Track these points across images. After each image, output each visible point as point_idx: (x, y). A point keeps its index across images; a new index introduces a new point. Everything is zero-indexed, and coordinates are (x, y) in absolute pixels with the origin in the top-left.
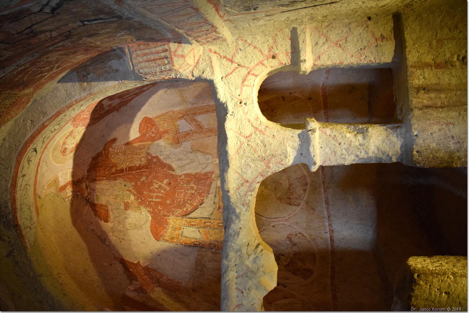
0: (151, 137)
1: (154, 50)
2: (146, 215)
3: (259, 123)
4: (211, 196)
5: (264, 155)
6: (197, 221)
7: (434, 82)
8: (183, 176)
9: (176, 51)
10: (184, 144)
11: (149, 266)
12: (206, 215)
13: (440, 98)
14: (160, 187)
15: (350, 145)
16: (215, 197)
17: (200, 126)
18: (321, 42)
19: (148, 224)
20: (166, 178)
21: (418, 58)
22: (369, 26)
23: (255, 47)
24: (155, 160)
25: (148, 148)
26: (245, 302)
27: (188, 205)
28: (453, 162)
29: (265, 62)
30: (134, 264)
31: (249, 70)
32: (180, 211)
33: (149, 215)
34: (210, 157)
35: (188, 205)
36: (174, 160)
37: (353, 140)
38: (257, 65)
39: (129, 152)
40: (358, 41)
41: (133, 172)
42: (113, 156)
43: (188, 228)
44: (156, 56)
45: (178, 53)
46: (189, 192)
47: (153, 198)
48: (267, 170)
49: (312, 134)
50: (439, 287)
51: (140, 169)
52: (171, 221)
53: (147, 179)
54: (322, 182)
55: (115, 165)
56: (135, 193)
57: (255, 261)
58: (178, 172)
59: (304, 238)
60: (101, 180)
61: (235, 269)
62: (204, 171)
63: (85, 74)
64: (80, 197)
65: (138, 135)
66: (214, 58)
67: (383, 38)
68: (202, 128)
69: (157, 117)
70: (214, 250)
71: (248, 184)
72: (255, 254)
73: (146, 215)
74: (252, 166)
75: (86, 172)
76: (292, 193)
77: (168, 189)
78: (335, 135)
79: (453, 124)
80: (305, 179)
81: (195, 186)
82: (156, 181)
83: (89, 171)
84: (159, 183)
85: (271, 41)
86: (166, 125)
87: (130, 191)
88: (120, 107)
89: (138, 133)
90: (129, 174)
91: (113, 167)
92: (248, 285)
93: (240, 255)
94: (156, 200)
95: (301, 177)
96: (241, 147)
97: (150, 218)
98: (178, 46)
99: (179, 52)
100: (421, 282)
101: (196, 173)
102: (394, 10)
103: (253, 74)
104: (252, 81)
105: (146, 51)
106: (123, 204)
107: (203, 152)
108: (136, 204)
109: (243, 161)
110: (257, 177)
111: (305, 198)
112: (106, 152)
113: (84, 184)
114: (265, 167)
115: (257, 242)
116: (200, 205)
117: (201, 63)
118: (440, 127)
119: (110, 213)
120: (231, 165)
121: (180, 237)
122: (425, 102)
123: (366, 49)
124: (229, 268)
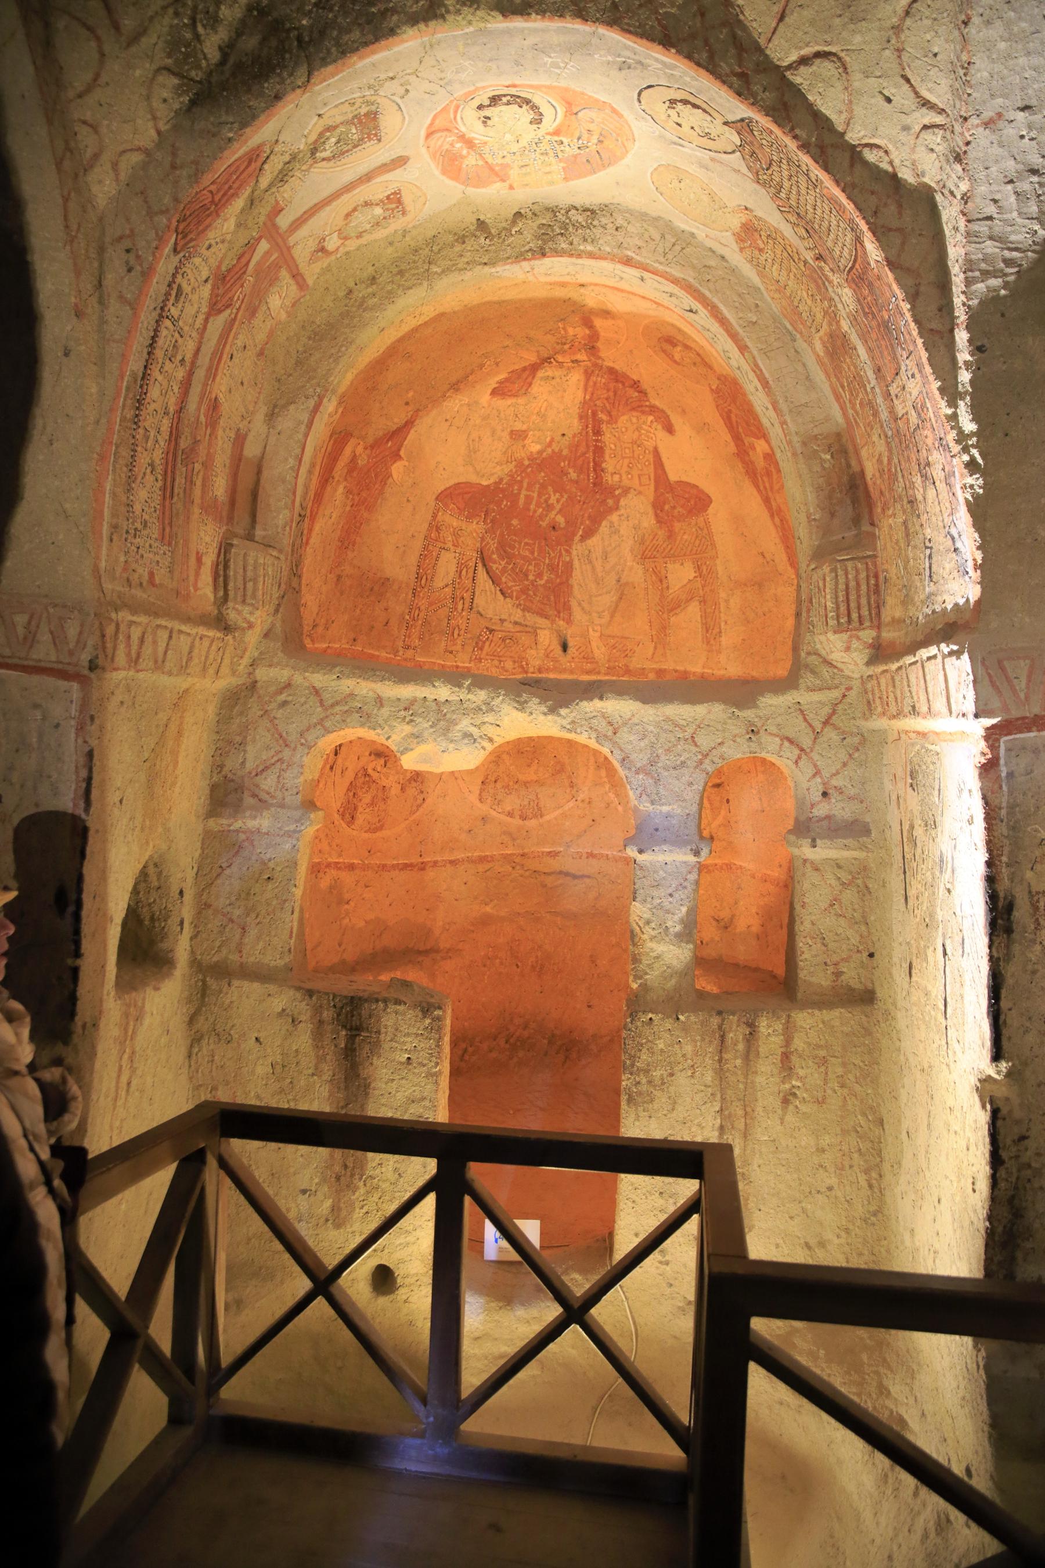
0: (664, 504)
1: (864, 601)
2: (493, 474)
3: (716, 760)
4: (518, 615)
5: (659, 765)
6: (468, 583)
7: (760, 1049)
8: (568, 559)
9: (858, 638)
10: (639, 570)
11: (390, 480)
12: (480, 601)
13: (736, 1058)
14: (550, 507)
15: (668, 912)
16: (516, 623)
17: (676, 606)
18: (842, 874)
19: (473, 479)
20: (567, 522)
21: (802, 1027)
22: (859, 955)
23: (845, 765)
24: (610, 502)
25: (640, 493)
26: (385, 711)
27: (503, 563)
28: (631, 1074)
29: (818, 780)
30: (399, 450)
31: (808, 750)
32: (493, 547)
33: (492, 481)
34: (604, 621)
35: (503, 563)
36: (606, 543)
37: (676, 918)
38: (815, 766)
39: (636, 453)
40: (837, 934)
41: (590, 455)
42: (634, 420)
43: (455, 561)
44: (853, 605)
45: (854, 641)
46: (530, 567)
47: (528, 490)
48: (633, 769)
49: (691, 850)
50: (419, 1048)
51: (595, 470)
52: (474, 526)
53: (571, 480)
54: (526, 851)
55: (612, 420)
56: (545, 454)
57: (467, 735)
58: (578, 549)
59: (415, 808)
60: (586, 389)
61: (454, 698)
62: (574, 603)
63: (833, 450)
64: (558, 347)
65: (673, 477)
66: (836, 694)
67: (838, 974)
68: (672, 610)
69: (707, 523)
70: (407, 617)
71: (610, 733)
72: (481, 737)
73: (493, 474)
74: (642, 744)
75: (611, 364)
76: (507, 787)
77: (544, 524)
78: (685, 887)
79: (692, 1077)
80: (535, 816)
81: (542, 582)
82: (564, 499)
83: (611, 371)
84: (558, 507)
85: (853, 792)
86: (685, 537)
87: (550, 445)
88: (743, 462)
89: (676, 479)
90: (588, 446)
91: (609, 414)
92: (421, 720)
93: (481, 709)
94: (522, 496)
95: (539, 809)
96: (676, 726)
97: (485, 483)
98: (865, 643)
99: (855, 644)
100: (428, 1021)
101: (570, 587)
102: (879, 994)
103: (799, 758)
104: (789, 755)
105: (864, 587)
106: (525, 427)
107: (617, 606)
108: (521, 454)
109: (651, 728)
110: (621, 750)
111: (494, 813)
112: (647, 409)
113: (585, 358)
114: (639, 765)
115: (496, 738)
116: (501, 590)
117: (830, 670)
118: (689, 1056)
119: (510, 401)
120: (647, 707)
121: (439, 545)
122: (731, 1035)
123: (824, 948)
124: (457, 689)
